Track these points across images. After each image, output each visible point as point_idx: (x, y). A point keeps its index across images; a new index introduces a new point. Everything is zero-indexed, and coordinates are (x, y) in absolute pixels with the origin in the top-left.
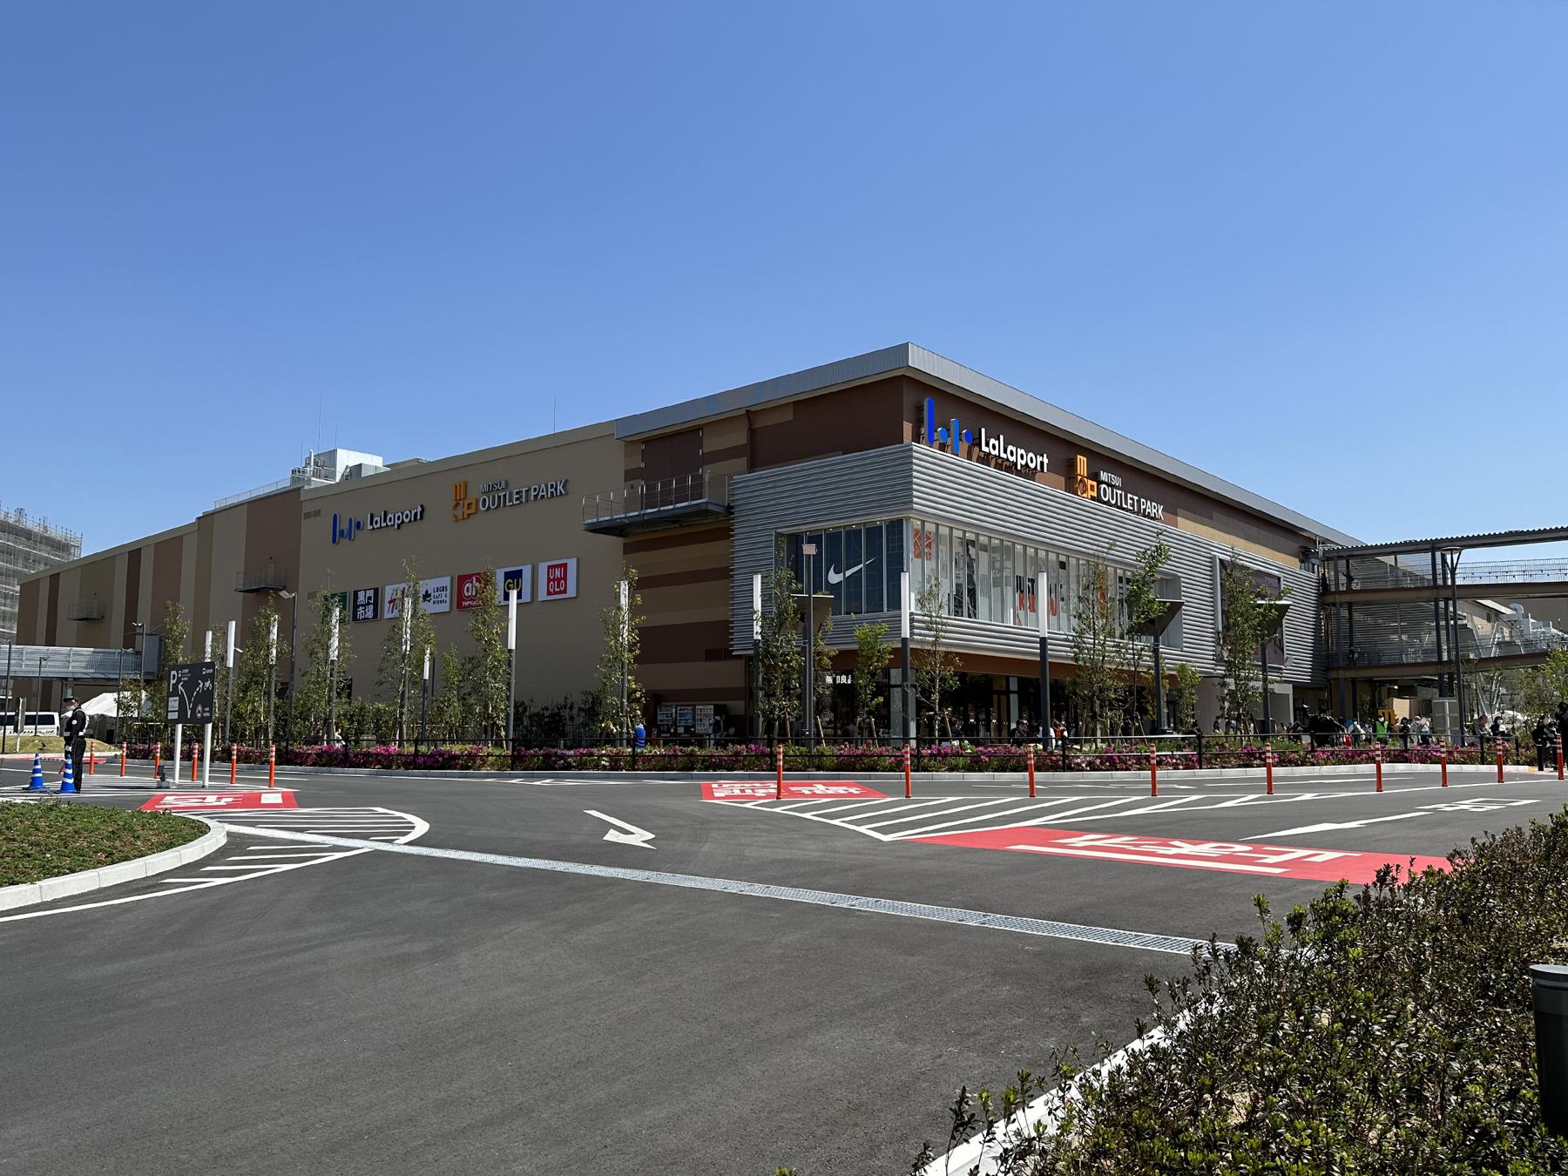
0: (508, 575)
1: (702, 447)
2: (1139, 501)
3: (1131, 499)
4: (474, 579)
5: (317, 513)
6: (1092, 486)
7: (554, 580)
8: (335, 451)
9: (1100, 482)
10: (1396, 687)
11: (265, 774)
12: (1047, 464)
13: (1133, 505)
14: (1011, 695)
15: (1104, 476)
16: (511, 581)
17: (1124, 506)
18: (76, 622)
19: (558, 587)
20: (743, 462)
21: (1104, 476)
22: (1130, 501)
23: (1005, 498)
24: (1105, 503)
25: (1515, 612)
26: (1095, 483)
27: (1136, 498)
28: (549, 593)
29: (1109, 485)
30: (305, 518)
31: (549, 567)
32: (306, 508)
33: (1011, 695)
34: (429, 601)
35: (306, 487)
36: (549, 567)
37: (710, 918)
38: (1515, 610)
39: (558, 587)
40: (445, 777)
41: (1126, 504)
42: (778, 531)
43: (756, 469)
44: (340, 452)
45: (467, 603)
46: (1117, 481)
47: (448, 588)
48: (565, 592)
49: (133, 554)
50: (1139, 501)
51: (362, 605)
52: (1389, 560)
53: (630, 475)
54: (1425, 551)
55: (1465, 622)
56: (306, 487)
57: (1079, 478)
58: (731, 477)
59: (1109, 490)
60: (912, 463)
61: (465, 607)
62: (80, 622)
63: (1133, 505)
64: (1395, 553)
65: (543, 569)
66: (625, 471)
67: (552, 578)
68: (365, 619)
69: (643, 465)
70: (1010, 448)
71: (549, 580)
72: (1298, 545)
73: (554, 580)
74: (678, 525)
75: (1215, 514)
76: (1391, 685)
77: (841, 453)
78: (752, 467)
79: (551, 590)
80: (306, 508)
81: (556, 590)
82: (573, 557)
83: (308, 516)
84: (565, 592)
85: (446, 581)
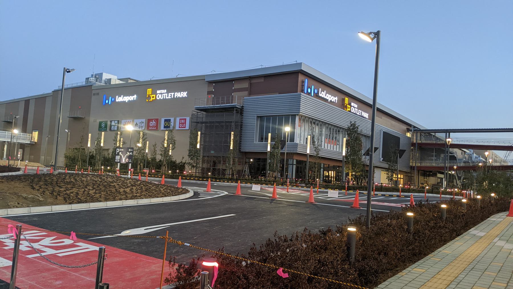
0: (165, 120)
1: (234, 87)
2: (362, 112)
3: (360, 111)
4: (154, 121)
5: (98, 94)
6: (349, 107)
7: (181, 123)
8: (102, 73)
9: (351, 106)
10: (431, 173)
11: (374, 206)
12: (337, 100)
13: (360, 113)
14: (294, 165)
15: (352, 104)
16: (166, 122)
17: (357, 114)
18: (3, 122)
19: (183, 126)
20: (246, 93)
21: (352, 104)
22: (359, 112)
23: (347, 120)
24: (352, 113)
25: (470, 152)
26: (350, 106)
27: (361, 111)
28: (180, 127)
29: (354, 107)
30: (93, 95)
31: (180, 119)
32: (93, 92)
33: (294, 165)
34: (137, 126)
35: (94, 85)
36: (180, 119)
37: (266, 236)
38: (470, 151)
39: (183, 126)
40: (280, 199)
41: (358, 113)
42: (444, 179)
43: (251, 95)
44: (104, 74)
45: (151, 128)
46: (356, 106)
47: (144, 123)
48: (185, 127)
49: (27, 102)
50: (362, 112)
51: (113, 126)
52: (433, 134)
53: (209, 93)
54: (444, 132)
55: (454, 154)
56: (94, 85)
57: (345, 104)
58: (243, 98)
59: (353, 109)
60: (301, 99)
61: (150, 129)
62: (5, 122)
63: (360, 113)
64: (435, 132)
65: (178, 119)
66: (208, 92)
67: (181, 123)
68: (114, 130)
69: (213, 90)
70: (327, 95)
71: (180, 123)
72: (406, 128)
73: (181, 123)
74: (224, 110)
75: (383, 117)
76: (430, 172)
77: (278, 93)
78: (250, 94)
79: (181, 127)
80: (93, 92)
81: (182, 126)
82: (188, 117)
83: (94, 94)
84: (185, 127)
85: (144, 120)
